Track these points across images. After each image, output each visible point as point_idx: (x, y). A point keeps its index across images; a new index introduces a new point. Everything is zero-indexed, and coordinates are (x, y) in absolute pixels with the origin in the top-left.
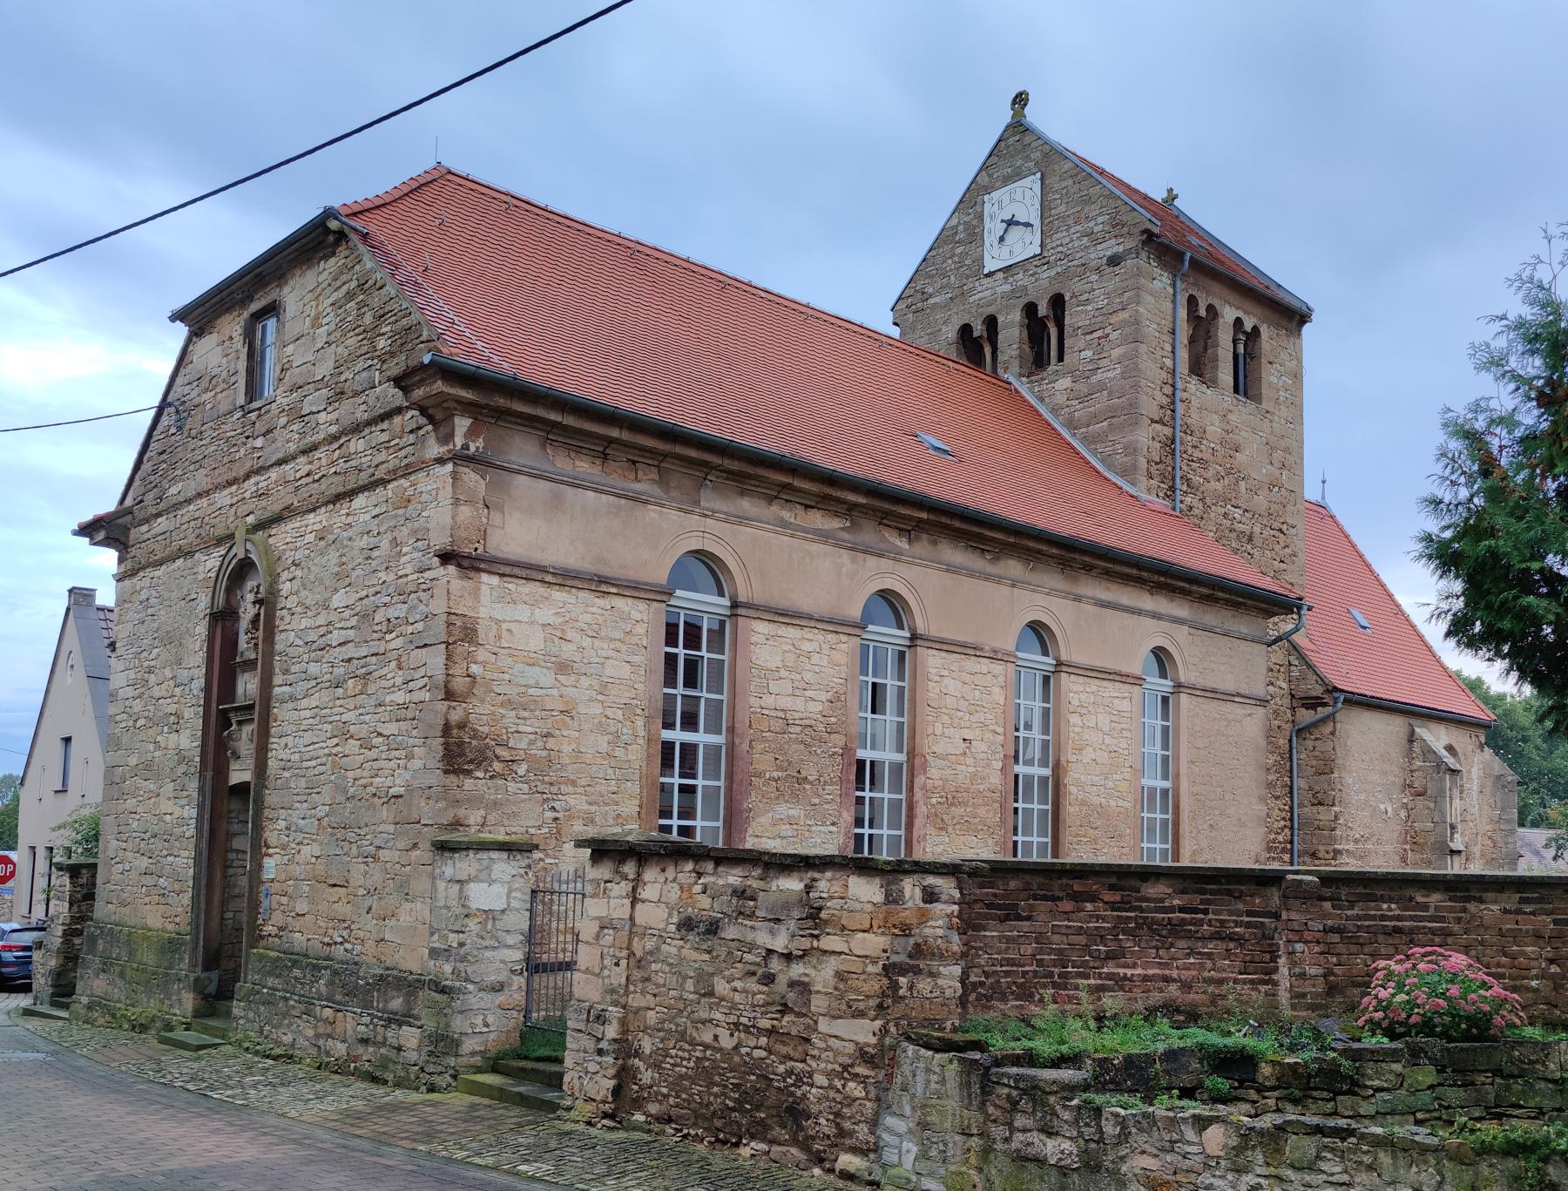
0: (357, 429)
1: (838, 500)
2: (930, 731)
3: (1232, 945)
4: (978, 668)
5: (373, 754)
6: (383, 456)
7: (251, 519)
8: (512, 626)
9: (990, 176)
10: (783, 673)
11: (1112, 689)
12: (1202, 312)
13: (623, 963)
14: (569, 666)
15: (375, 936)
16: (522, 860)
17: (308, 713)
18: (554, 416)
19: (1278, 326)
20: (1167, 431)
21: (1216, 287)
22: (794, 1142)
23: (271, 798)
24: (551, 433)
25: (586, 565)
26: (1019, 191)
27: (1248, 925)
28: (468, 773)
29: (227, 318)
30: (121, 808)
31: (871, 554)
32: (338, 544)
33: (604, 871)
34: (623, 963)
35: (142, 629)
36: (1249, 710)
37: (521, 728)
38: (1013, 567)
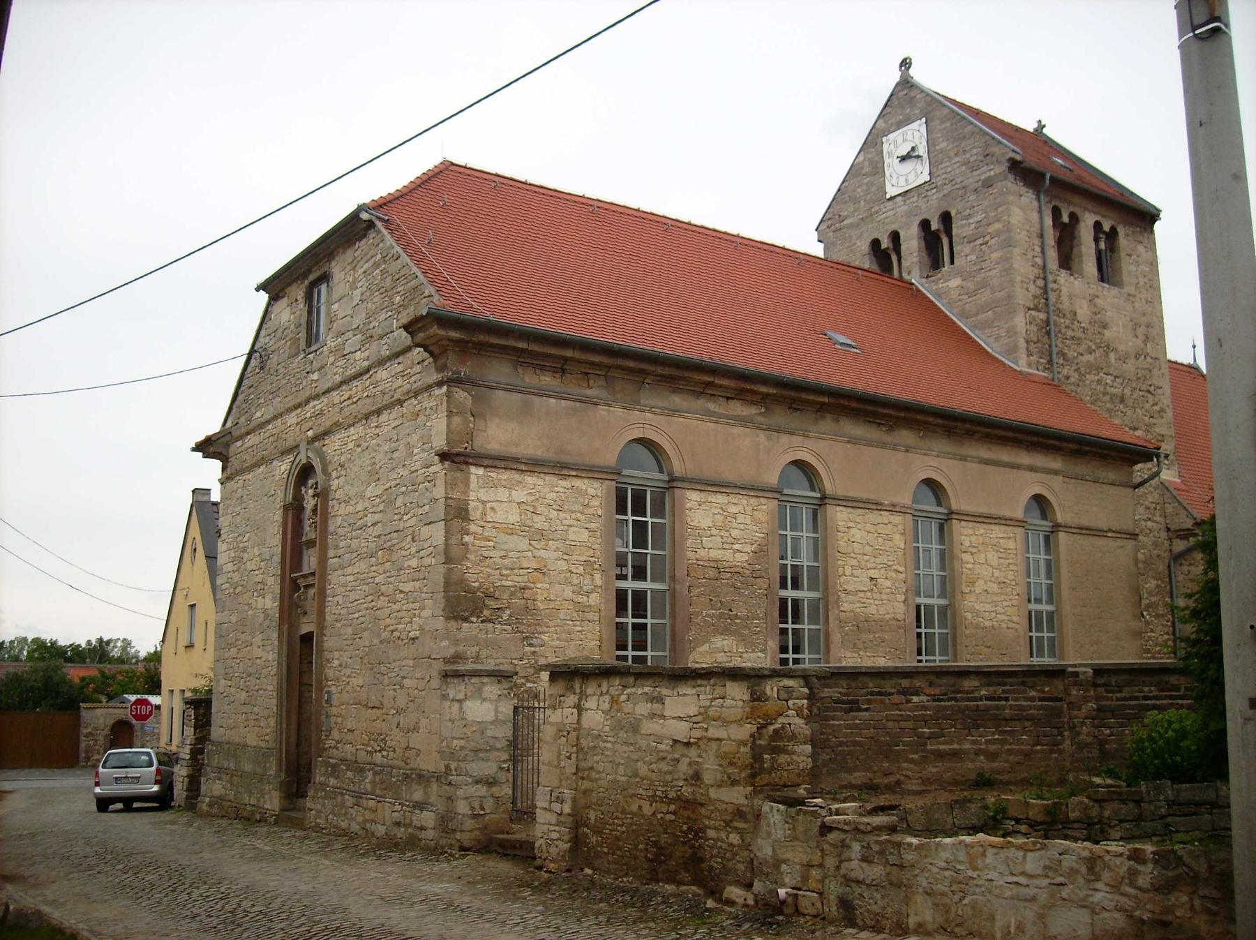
0: (382, 362)
1: (754, 392)
2: (841, 570)
3: (1027, 724)
4: (880, 519)
5: (396, 607)
6: (400, 382)
7: (310, 433)
8: (494, 505)
9: (886, 122)
10: (714, 531)
11: (997, 532)
12: (1066, 219)
13: (574, 756)
14: (544, 534)
15: (404, 745)
16: (505, 685)
17: (351, 578)
18: (522, 345)
19: (1132, 225)
20: (1042, 316)
21: (1076, 199)
22: (695, 882)
23: (329, 643)
24: (521, 359)
25: (551, 455)
26: (910, 133)
27: (1041, 708)
28: (465, 620)
29: (295, 286)
30: (227, 655)
31: (784, 432)
32: (370, 450)
33: (559, 688)
34: (574, 756)
35: (238, 519)
36: (1120, 543)
37: (504, 583)
38: (906, 436)
